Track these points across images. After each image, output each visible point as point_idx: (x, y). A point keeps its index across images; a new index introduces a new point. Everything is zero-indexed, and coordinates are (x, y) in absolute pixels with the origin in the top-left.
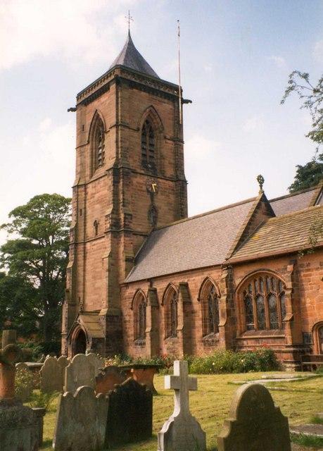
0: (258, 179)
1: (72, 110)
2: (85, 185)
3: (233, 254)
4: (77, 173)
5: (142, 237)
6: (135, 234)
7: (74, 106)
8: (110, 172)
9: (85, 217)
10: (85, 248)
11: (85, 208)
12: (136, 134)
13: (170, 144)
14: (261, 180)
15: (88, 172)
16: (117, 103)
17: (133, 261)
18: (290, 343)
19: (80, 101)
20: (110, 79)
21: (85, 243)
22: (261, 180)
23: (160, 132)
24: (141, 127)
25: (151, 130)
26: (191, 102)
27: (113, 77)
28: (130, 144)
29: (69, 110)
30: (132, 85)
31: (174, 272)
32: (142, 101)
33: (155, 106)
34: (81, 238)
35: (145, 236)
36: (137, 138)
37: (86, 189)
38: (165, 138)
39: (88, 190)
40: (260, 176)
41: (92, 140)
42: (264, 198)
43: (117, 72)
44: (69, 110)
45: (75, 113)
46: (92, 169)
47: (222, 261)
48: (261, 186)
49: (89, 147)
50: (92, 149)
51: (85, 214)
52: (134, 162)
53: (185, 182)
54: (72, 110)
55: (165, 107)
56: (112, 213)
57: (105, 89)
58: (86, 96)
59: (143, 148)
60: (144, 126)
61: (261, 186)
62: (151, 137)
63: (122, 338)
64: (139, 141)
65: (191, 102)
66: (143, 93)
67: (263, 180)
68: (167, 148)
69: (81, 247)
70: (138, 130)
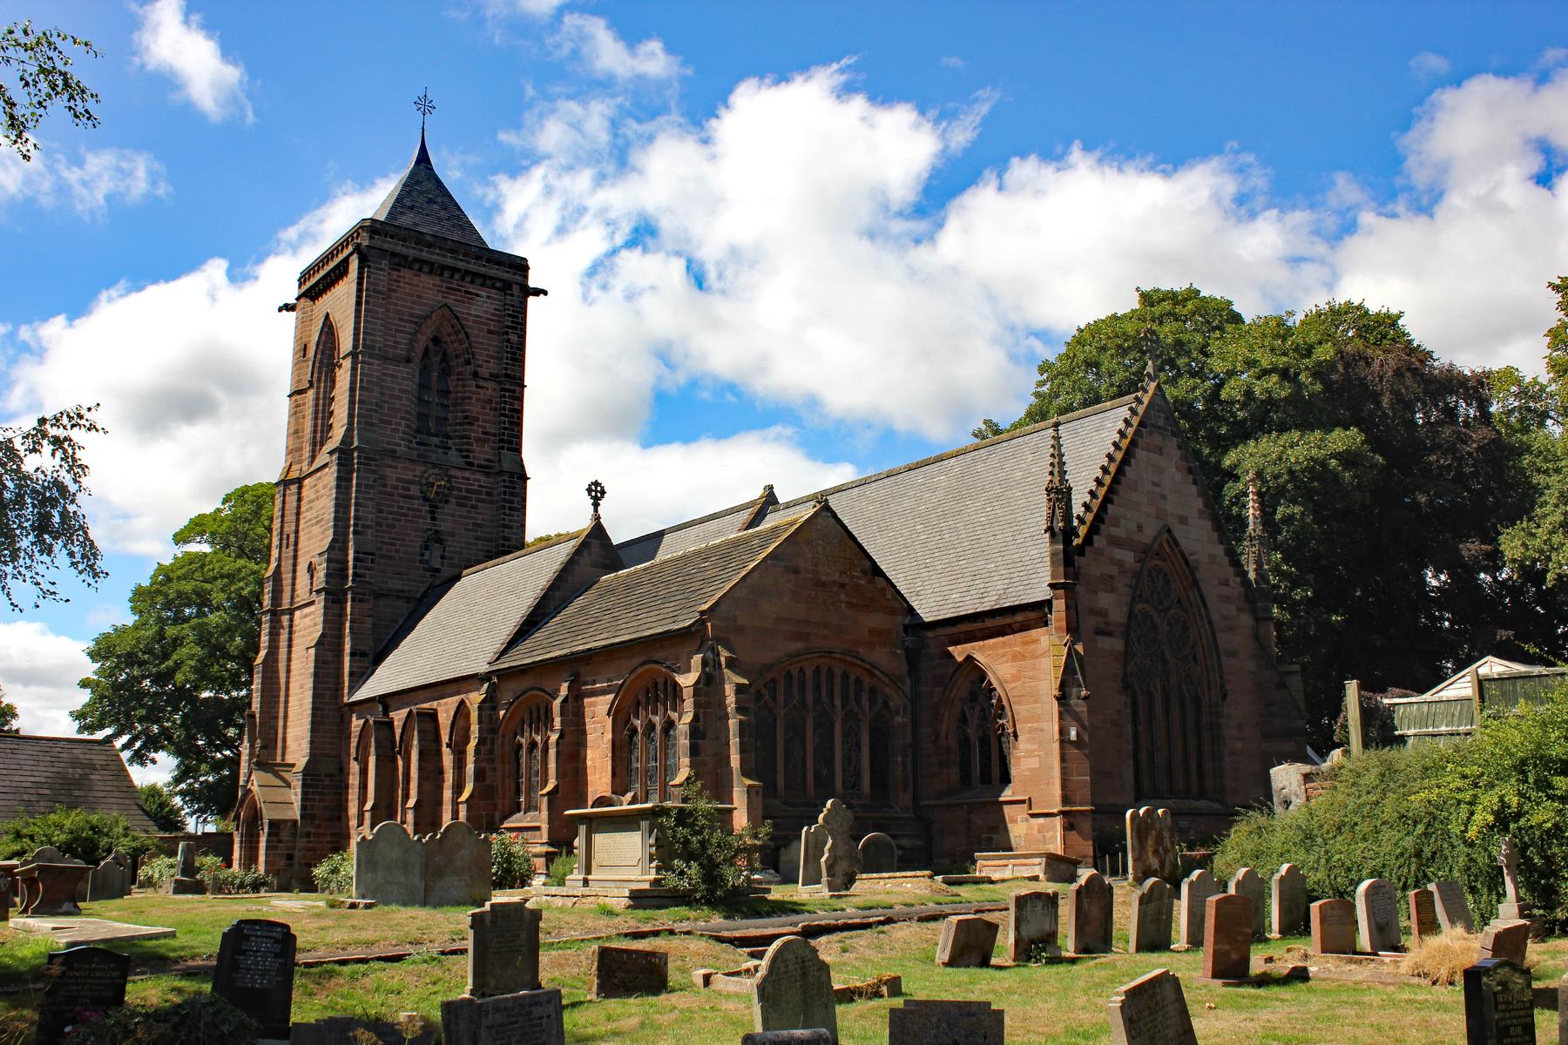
0: (589, 490)
1: (288, 308)
2: (299, 481)
3: (503, 652)
4: (289, 452)
5: (401, 603)
6: (379, 595)
7: (292, 301)
8: (336, 456)
9: (296, 551)
10: (291, 620)
11: (297, 532)
12: (403, 370)
13: (490, 389)
14: (596, 492)
15: (306, 453)
16: (358, 303)
17: (372, 657)
18: (545, 840)
19: (305, 288)
20: (346, 252)
21: (291, 612)
22: (596, 492)
23: (468, 362)
24: (420, 351)
25: (445, 359)
26: (545, 293)
27: (350, 248)
28: (382, 394)
29: (280, 310)
30: (400, 262)
31: (291, 692)
32: (426, 290)
33: (460, 309)
34: (286, 604)
35: (408, 600)
36: (405, 380)
37: (300, 488)
38: (476, 375)
39: (305, 492)
40: (596, 484)
41: (319, 380)
42: (598, 531)
43: (364, 241)
44: (280, 310)
45: (293, 315)
46: (314, 444)
47: (483, 668)
48: (596, 505)
49: (311, 394)
50: (317, 399)
51: (296, 544)
52: (397, 435)
53: (520, 477)
54: (288, 308)
55: (483, 306)
56: (331, 548)
57: (340, 272)
58: (313, 281)
59: (420, 399)
60: (427, 350)
61: (596, 505)
62: (446, 373)
63: (339, 819)
64: (411, 385)
65: (545, 293)
66: (424, 277)
67: (603, 492)
68: (479, 400)
69: (285, 619)
70: (409, 361)
